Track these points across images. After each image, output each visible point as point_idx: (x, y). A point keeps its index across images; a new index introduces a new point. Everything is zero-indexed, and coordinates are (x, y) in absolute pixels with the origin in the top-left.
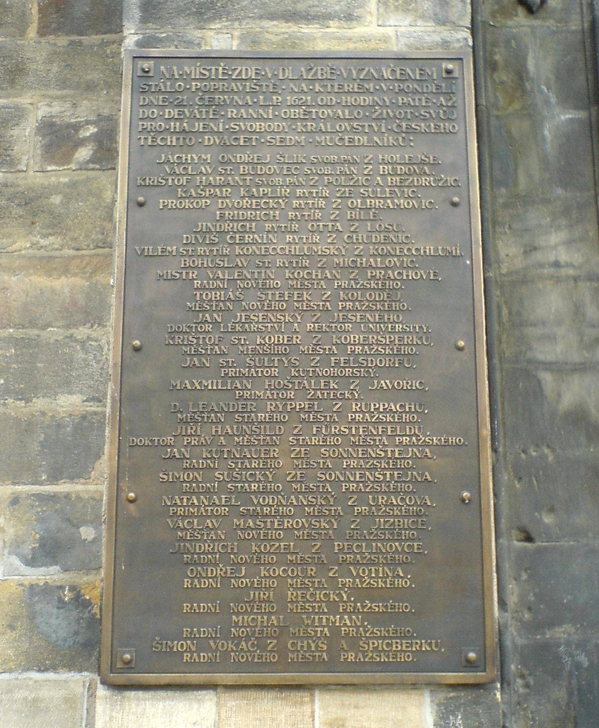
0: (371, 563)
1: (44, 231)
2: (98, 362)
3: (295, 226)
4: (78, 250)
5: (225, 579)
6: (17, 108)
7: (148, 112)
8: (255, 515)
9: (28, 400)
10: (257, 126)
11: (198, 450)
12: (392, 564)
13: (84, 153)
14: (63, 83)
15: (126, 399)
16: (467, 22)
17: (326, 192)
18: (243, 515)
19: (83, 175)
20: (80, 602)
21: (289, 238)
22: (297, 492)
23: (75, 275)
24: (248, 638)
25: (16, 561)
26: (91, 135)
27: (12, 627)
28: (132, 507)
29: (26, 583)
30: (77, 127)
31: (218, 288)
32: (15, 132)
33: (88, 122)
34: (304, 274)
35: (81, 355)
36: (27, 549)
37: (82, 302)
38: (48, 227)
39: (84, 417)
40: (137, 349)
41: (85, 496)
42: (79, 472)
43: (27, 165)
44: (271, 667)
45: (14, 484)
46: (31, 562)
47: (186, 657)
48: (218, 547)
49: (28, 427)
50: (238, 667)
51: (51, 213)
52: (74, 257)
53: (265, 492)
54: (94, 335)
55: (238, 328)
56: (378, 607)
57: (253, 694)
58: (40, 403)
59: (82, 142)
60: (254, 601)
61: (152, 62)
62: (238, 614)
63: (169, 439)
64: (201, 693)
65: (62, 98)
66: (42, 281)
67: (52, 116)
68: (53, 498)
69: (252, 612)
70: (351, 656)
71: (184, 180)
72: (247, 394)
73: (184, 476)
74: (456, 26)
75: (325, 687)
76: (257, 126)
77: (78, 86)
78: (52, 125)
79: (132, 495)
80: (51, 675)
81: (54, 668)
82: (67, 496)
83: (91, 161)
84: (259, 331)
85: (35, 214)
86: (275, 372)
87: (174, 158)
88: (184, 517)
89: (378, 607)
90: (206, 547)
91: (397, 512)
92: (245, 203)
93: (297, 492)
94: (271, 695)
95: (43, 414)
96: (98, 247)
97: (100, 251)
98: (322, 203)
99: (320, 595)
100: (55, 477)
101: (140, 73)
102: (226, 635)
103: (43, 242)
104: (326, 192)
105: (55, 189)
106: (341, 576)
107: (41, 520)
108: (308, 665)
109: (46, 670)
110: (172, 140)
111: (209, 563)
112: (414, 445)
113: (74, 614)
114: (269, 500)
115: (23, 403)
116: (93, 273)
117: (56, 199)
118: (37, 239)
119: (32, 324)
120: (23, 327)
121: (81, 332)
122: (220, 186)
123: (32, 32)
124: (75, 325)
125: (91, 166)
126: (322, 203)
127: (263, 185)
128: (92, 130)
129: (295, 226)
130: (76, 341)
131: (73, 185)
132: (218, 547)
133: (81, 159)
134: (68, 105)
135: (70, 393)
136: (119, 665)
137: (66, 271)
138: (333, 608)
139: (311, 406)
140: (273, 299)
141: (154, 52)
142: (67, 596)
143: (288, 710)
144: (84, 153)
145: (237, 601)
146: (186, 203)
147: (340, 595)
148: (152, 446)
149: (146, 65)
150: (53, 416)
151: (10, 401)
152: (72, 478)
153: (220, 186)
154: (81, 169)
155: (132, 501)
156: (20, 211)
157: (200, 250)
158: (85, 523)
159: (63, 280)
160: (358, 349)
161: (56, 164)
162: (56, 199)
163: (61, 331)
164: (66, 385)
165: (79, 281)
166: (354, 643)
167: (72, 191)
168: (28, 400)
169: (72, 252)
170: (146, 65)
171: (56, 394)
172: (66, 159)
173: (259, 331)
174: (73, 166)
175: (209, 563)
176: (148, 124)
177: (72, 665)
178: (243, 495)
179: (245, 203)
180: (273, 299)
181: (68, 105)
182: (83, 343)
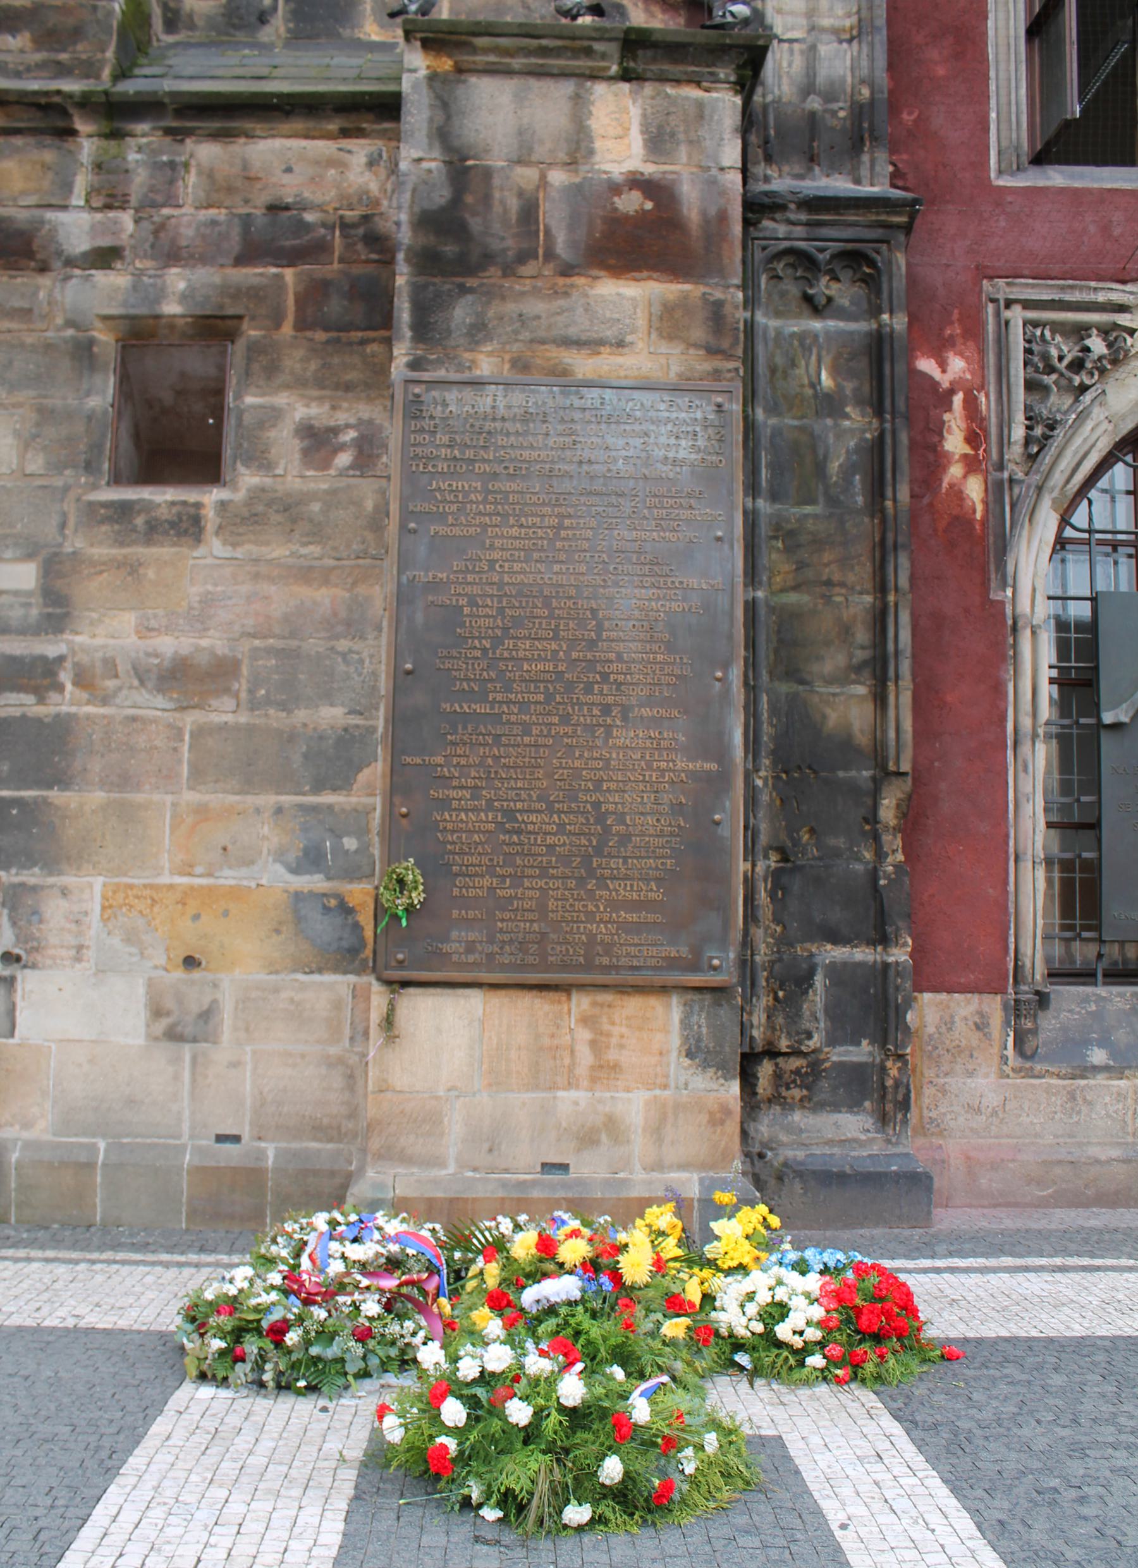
0: (627, 878)
1: (305, 539)
2: (360, 675)
3: (563, 556)
4: (338, 559)
5: (492, 889)
6: (273, 408)
7: (419, 439)
8: (519, 832)
9: (290, 712)
10: (526, 454)
11: (466, 770)
12: (646, 880)
13: (344, 459)
14: (320, 384)
15: (396, 719)
16: (740, 352)
17: (593, 523)
18: (508, 832)
19: (343, 482)
20: (346, 909)
21: (556, 567)
22: (560, 812)
23: (336, 586)
24: (511, 941)
25: (280, 869)
26: (353, 440)
27: (277, 931)
28: (404, 821)
29: (291, 890)
30: (335, 431)
31: (487, 616)
32: (272, 434)
33: (348, 426)
34: (570, 603)
35: (342, 668)
36: (291, 857)
37: (343, 614)
38: (308, 535)
39: (346, 730)
40: (408, 673)
41: (348, 808)
42: (343, 783)
43: (285, 470)
44: (533, 968)
45: (278, 793)
46: (296, 870)
47: (455, 958)
48: (485, 860)
49: (291, 738)
50: (504, 968)
51: (311, 521)
52: (334, 568)
53: (530, 811)
54: (356, 648)
55: (506, 654)
56: (633, 917)
57: (514, 994)
58: (301, 715)
59: (342, 447)
60: (517, 909)
61: (423, 386)
62: (503, 920)
63: (440, 760)
64: (468, 991)
65: (320, 399)
66: (305, 593)
67: (310, 418)
68: (314, 809)
69: (515, 920)
70: (605, 961)
71: (454, 507)
72: (513, 718)
73: (453, 794)
74: (729, 357)
75: (582, 987)
76: (526, 454)
77: (337, 387)
78: (310, 428)
79: (404, 810)
80: (316, 977)
81: (320, 971)
82: (330, 807)
83: (352, 467)
84: (526, 659)
85: (294, 521)
86: (541, 698)
87: (444, 486)
88: (453, 831)
89: (633, 917)
90: (474, 860)
91: (652, 831)
92: (515, 531)
93: (560, 812)
94: (534, 993)
95: (305, 725)
96: (358, 558)
97: (361, 562)
98: (590, 533)
99: (578, 905)
100: (319, 787)
101: (411, 398)
102: (491, 941)
103: (304, 551)
104: (593, 523)
105: (312, 496)
106: (599, 888)
107: (305, 829)
108: (565, 967)
109: (312, 972)
110: (442, 466)
111: (476, 875)
112: (670, 770)
113: (339, 920)
114: (532, 817)
115: (284, 714)
116: (355, 584)
117: (316, 507)
118: (294, 548)
119: (292, 635)
120: (284, 638)
121: (343, 645)
122: (490, 515)
123: (288, 329)
124: (337, 637)
125: (351, 473)
126: (590, 533)
127: (532, 515)
128: (352, 434)
129: (563, 556)
130: (338, 653)
131: (333, 492)
132: (485, 860)
133: (340, 465)
134: (327, 407)
135: (332, 705)
136: (394, 964)
137: (326, 582)
138: (590, 917)
139: (575, 731)
140: (540, 628)
141: (426, 376)
142: (333, 903)
143: (547, 1007)
144: (344, 459)
145: (503, 909)
146: (457, 531)
147: (597, 906)
148: (423, 765)
149: (417, 390)
150: (315, 729)
151: (272, 712)
152: (335, 789)
153: (490, 515)
154: (340, 475)
155: (404, 816)
156: (279, 518)
157: (470, 578)
158: (348, 834)
159: (324, 590)
160: (621, 678)
161: (316, 469)
162: (316, 507)
163: (321, 642)
164: (328, 697)
165: (342, 594)
166: (608, 948)
167: (331, 498)
168: (290, 712)
169: (332, 563)
170: (417, 390)
171: (317, 706)
172: (326, 465)
173: (526, 659)
174: (332, 472)
175: (476, 875)
176: (419, 450)
177: (337, 969)
178: (510, 814)
179: (515, 531)
180: (540, 628)
181: (327, 407)
182: (344, 655)
